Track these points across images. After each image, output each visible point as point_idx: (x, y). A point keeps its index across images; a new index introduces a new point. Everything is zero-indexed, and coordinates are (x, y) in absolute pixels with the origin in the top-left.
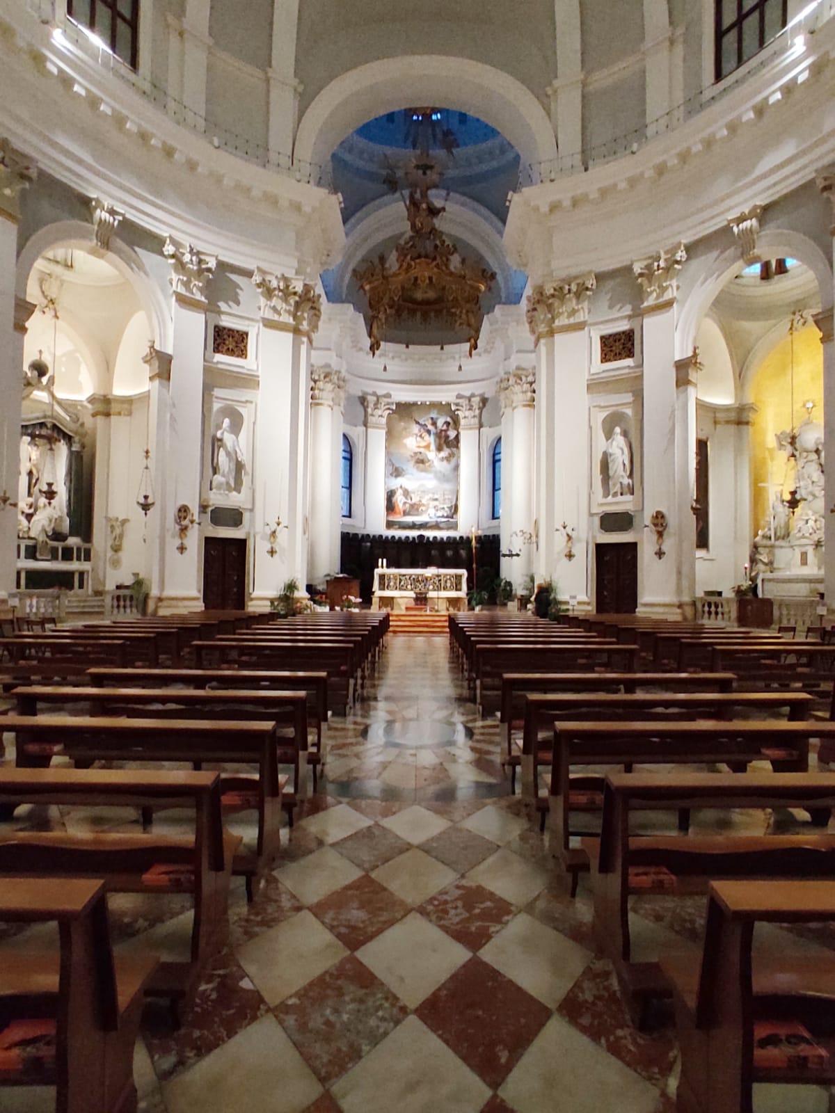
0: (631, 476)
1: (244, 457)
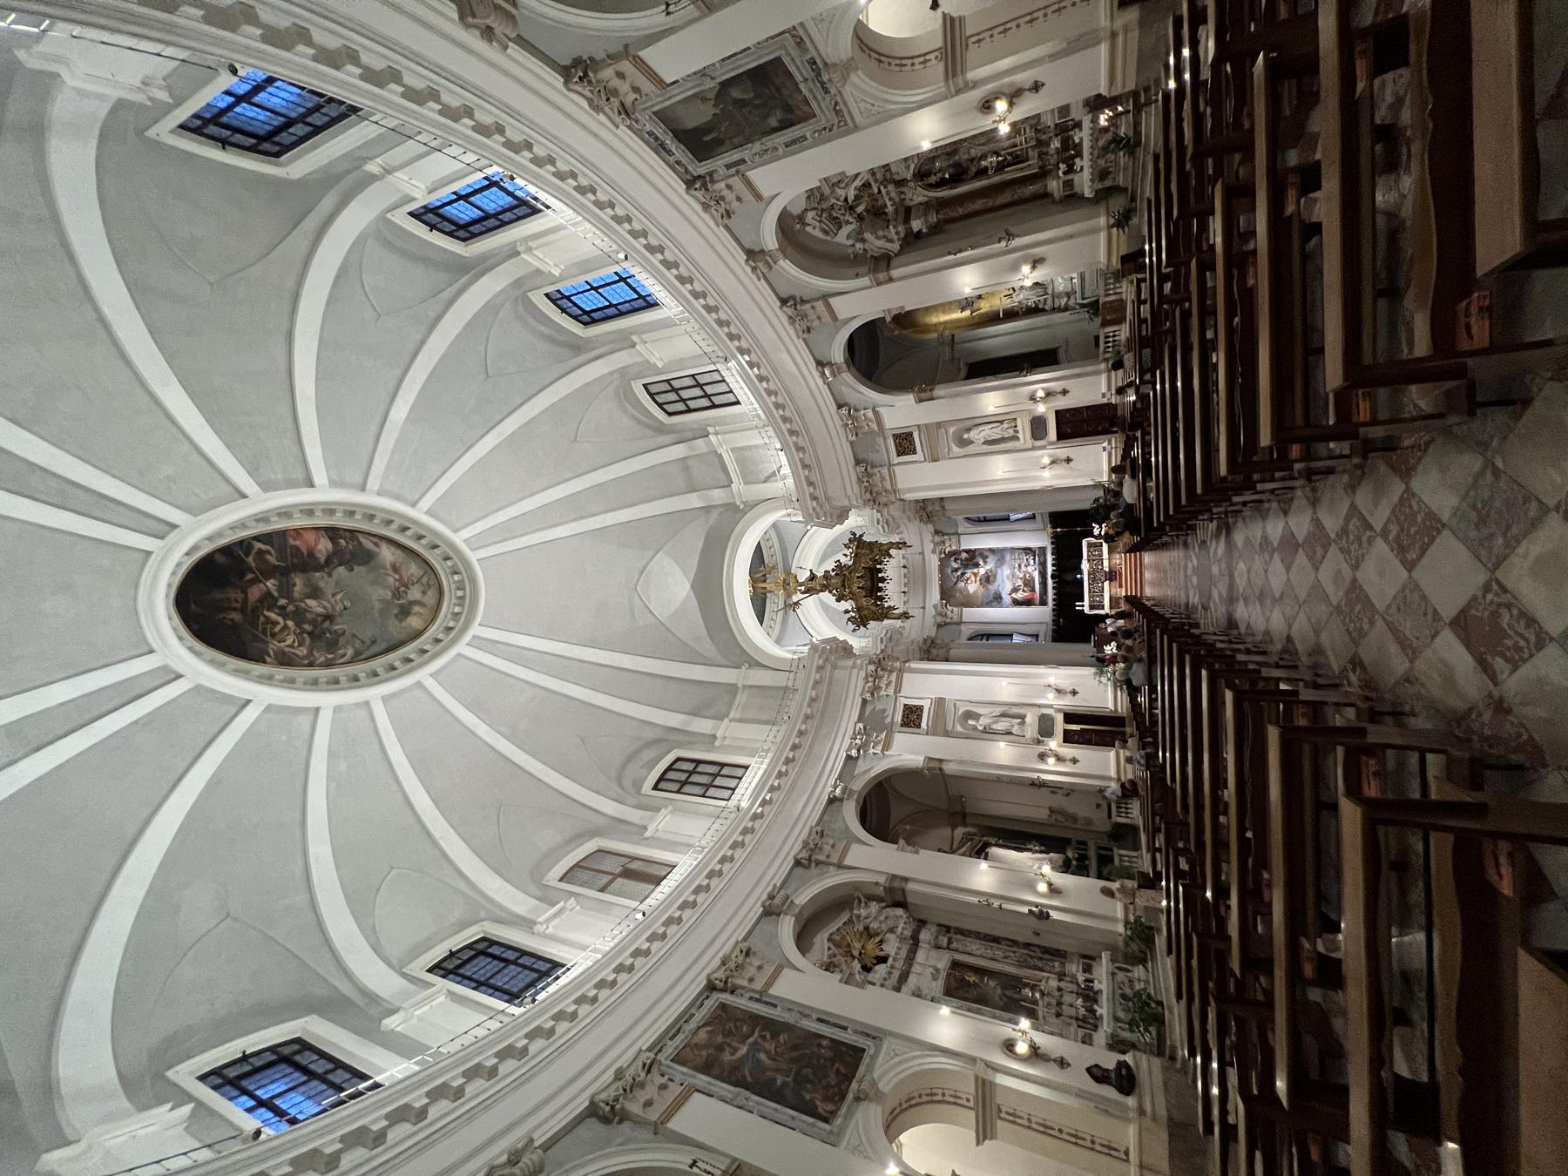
0: (1001, 422)
1: (998, 710)
